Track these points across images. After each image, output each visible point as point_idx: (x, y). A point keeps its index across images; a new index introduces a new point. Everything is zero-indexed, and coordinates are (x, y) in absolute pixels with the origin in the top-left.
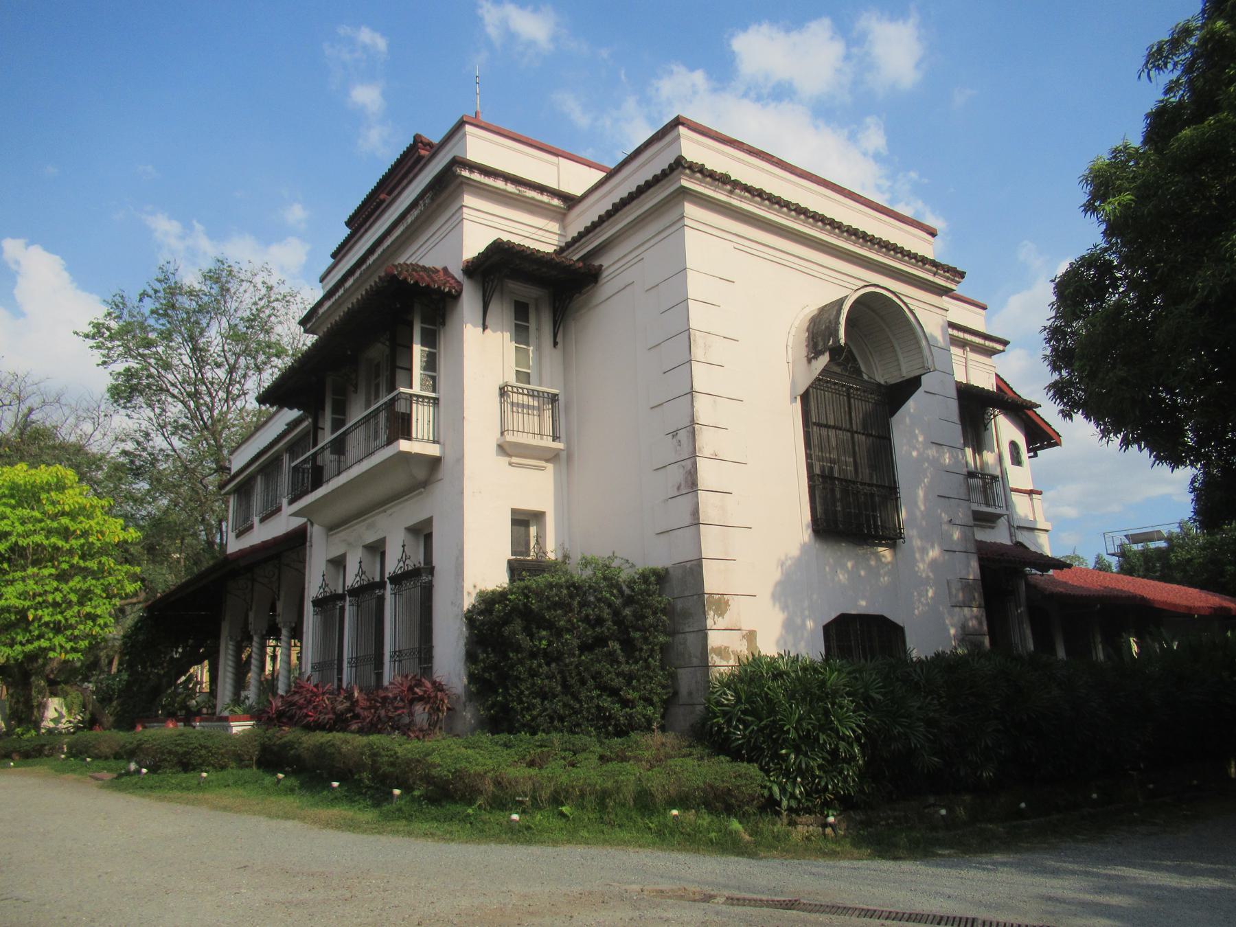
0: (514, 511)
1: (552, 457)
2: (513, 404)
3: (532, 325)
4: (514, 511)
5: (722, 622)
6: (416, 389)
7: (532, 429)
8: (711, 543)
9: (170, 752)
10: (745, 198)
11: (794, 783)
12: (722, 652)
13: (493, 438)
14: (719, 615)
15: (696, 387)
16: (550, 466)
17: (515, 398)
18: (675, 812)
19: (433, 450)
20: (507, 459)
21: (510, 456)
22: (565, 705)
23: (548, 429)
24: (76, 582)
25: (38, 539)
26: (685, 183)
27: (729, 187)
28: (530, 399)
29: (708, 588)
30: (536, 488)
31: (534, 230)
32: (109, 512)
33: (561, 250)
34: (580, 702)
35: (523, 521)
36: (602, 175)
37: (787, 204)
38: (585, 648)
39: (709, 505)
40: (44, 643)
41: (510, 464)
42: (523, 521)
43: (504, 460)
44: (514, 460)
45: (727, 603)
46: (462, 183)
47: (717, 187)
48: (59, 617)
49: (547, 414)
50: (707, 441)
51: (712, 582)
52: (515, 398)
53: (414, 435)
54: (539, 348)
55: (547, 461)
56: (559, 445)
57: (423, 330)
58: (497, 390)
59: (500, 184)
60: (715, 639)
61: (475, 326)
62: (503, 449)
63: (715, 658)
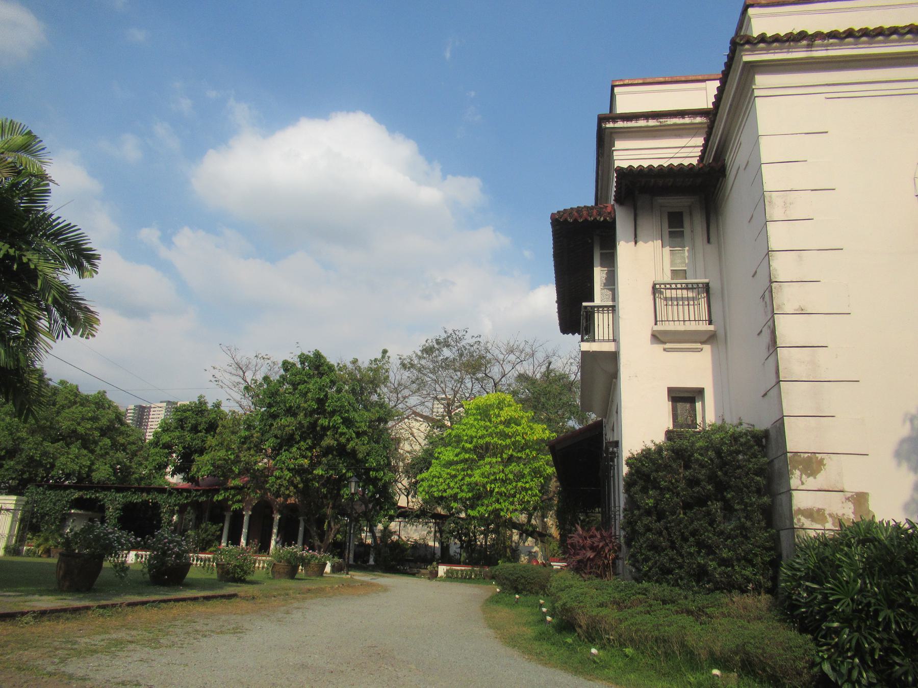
0: (671, 390)
1: (710, 338)
2: (666, 299)
3: (687, 229)
4: (671, 390)
5: (810, 482)
6: (598, 301)
7: (691, 317)
8: (794, 400)
9: (507, 579)
10: (831, 45)
11: (659, 648)
12: (814, 514)
13: (647, 326)
14: (809, 476)
15: (773, 245)
16: (707, 348)
17: (668, 293)
18: (716, 672)
19: (609, 347)
20: (661, 346)
21: (664, 343)
22: (672, 560)
23: (705, 316)
24: (513, 467)
25: (487, 439)
26: (746, 58)
27: (804, 42)
28: (685, 292)
29: (791, 446)
30: (695, 368)
31: (691, 149)
32: (533, 420)
33: (701, 158)
34: (682, 556)
35: (684, 398)
36: (717, 84)
37: (894, 31)
38: (687, 506)
39: (792, 362)
40: (498, 506)
41: (665, 350)
42: (684, 398)
43: (660, 347)
44: (668, 346)
45: (821, 463)
46: (611, 133)
47: (789, 48)
48: (503, 489)
49: (703, 302)
50: (788, 298)
51: (797, 439)
52: (668, 293)
53: (596, 338)
54: (693, 248)
55: (702, 343)
56: (711, 328)
57: (601, 254)
58: (651, 289)
59: (642, 123)
60: (801, 500)
61: (627, 242)
62: (657, 338)
63: (803, 519)
